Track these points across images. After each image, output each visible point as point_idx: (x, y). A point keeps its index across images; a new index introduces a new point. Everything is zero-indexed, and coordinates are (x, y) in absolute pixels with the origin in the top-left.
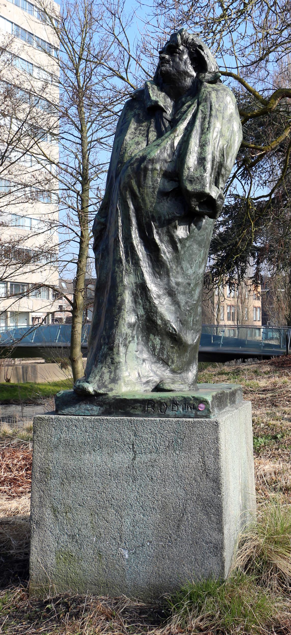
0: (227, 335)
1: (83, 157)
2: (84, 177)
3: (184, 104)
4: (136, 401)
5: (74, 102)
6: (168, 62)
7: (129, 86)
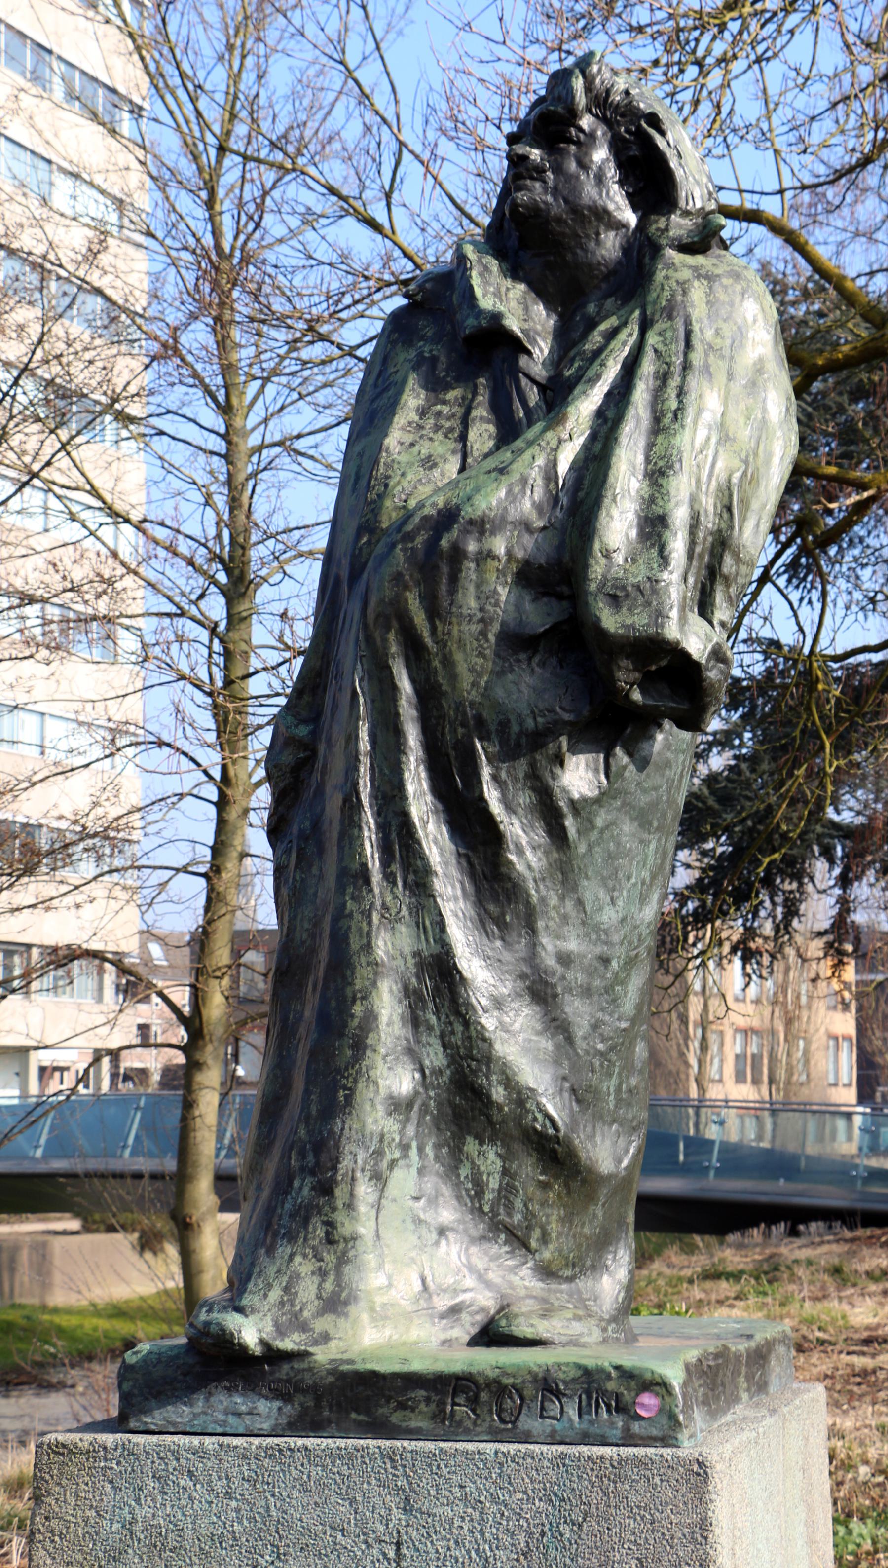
0: (734, 1137)
1: (234, 503)
2: (237, 572)
3: (592, 325)
4: (412, 1380)
5: (204, 307)
6: (538, 172)
7: (397, 253)
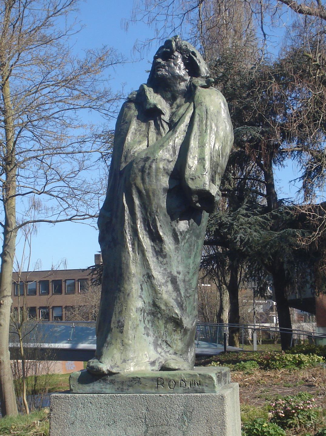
6: (164, 67)
